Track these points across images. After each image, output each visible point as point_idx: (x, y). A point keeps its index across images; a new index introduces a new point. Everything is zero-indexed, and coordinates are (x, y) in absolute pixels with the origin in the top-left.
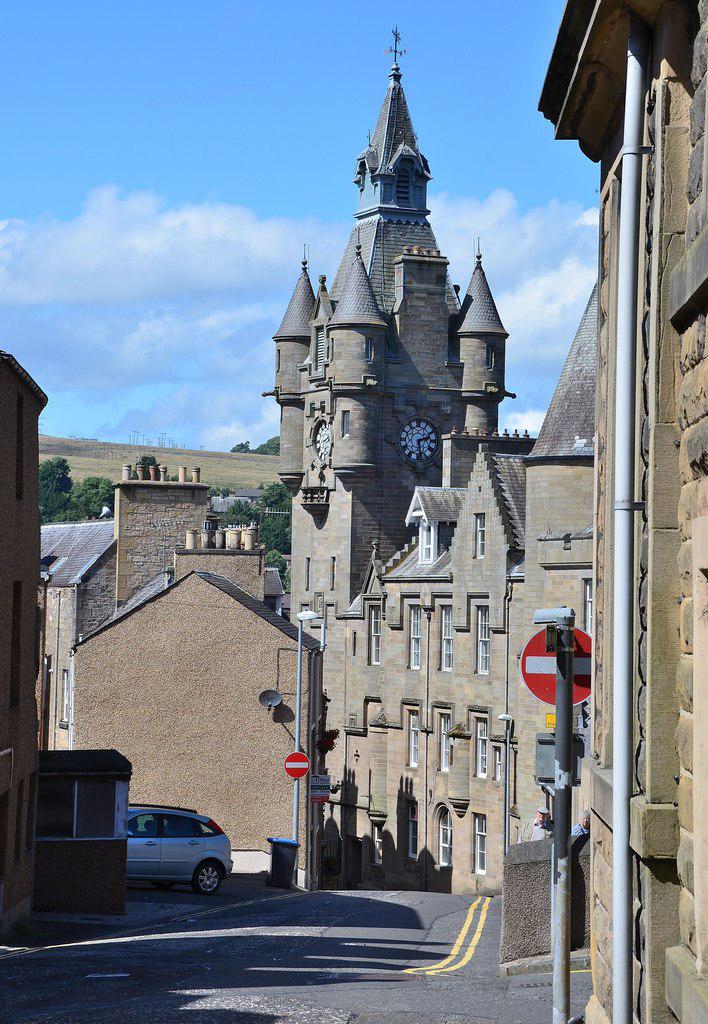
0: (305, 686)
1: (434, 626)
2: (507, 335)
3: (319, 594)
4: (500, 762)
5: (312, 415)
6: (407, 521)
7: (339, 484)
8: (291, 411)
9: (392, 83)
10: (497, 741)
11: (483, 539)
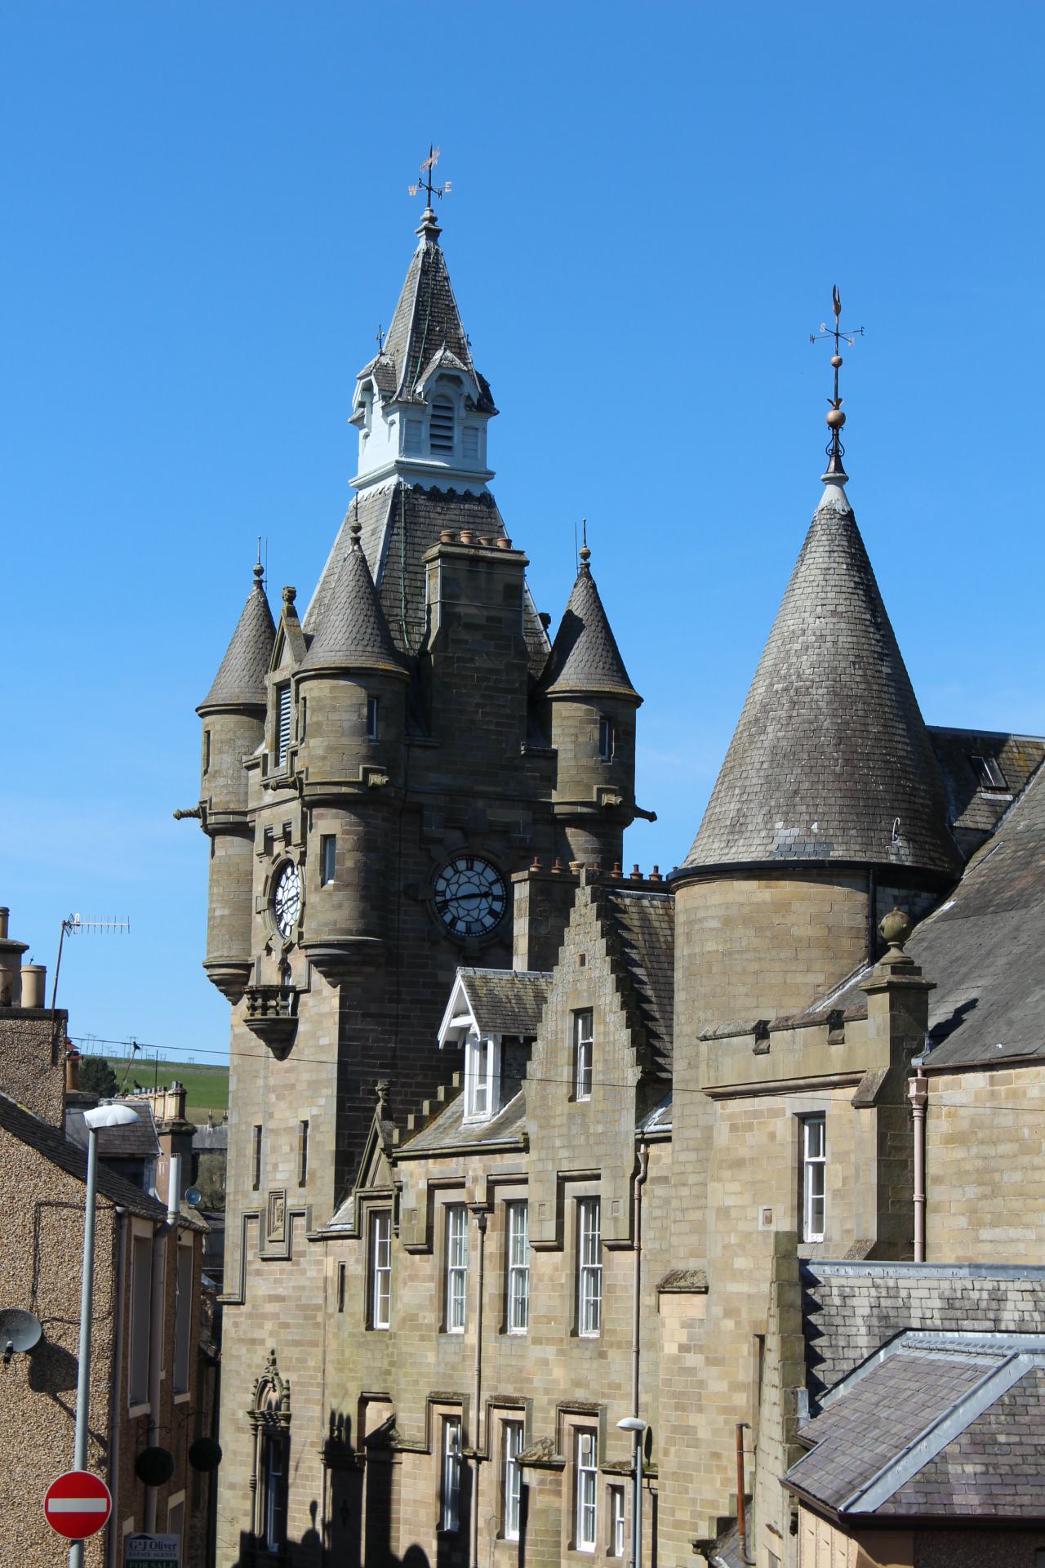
0: (103, 1301)
1: (492, 1245)
2: (638, 701)
3: (277, 1195)
4: (623, 1519)
5: (268, 850)
6: (442, 1037)
7: (318, 978)
8: (230, 845)
10: (619, 1474)
11: (589, 1062)
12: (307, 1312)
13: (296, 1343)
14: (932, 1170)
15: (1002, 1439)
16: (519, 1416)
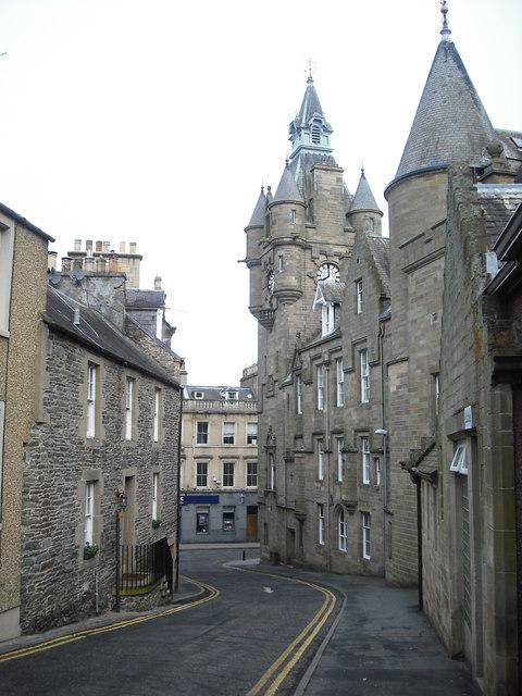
3: (271, 376)
16: (341, 436)
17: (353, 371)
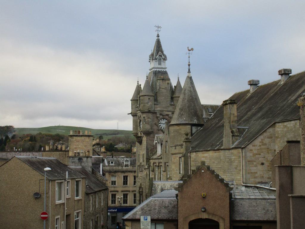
3: (141, 163)
9: (157, 38)
12: (144, 178)
13: (143, 182)
14: (191, 165)
15: (145, 209)
17: (165, 172)
